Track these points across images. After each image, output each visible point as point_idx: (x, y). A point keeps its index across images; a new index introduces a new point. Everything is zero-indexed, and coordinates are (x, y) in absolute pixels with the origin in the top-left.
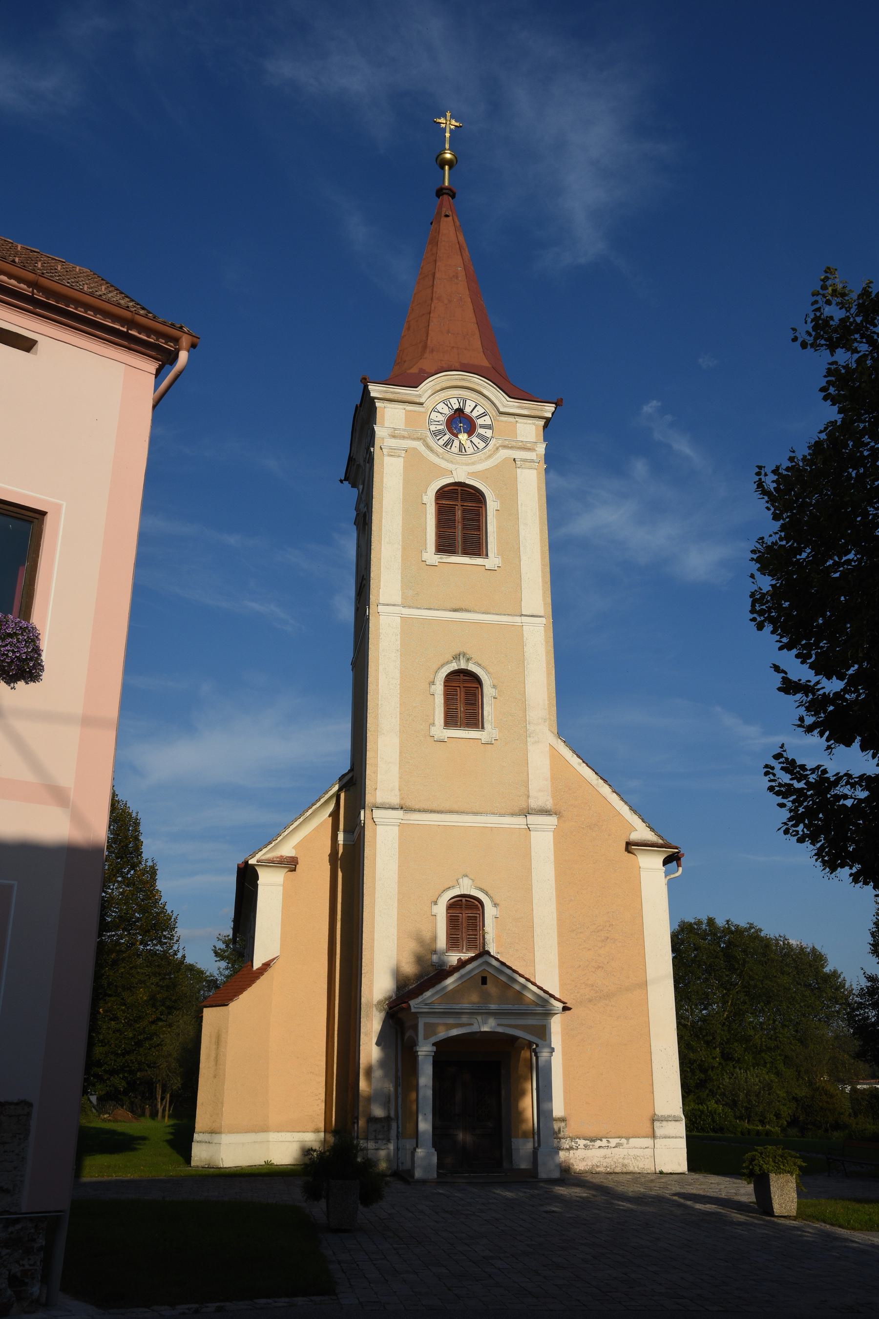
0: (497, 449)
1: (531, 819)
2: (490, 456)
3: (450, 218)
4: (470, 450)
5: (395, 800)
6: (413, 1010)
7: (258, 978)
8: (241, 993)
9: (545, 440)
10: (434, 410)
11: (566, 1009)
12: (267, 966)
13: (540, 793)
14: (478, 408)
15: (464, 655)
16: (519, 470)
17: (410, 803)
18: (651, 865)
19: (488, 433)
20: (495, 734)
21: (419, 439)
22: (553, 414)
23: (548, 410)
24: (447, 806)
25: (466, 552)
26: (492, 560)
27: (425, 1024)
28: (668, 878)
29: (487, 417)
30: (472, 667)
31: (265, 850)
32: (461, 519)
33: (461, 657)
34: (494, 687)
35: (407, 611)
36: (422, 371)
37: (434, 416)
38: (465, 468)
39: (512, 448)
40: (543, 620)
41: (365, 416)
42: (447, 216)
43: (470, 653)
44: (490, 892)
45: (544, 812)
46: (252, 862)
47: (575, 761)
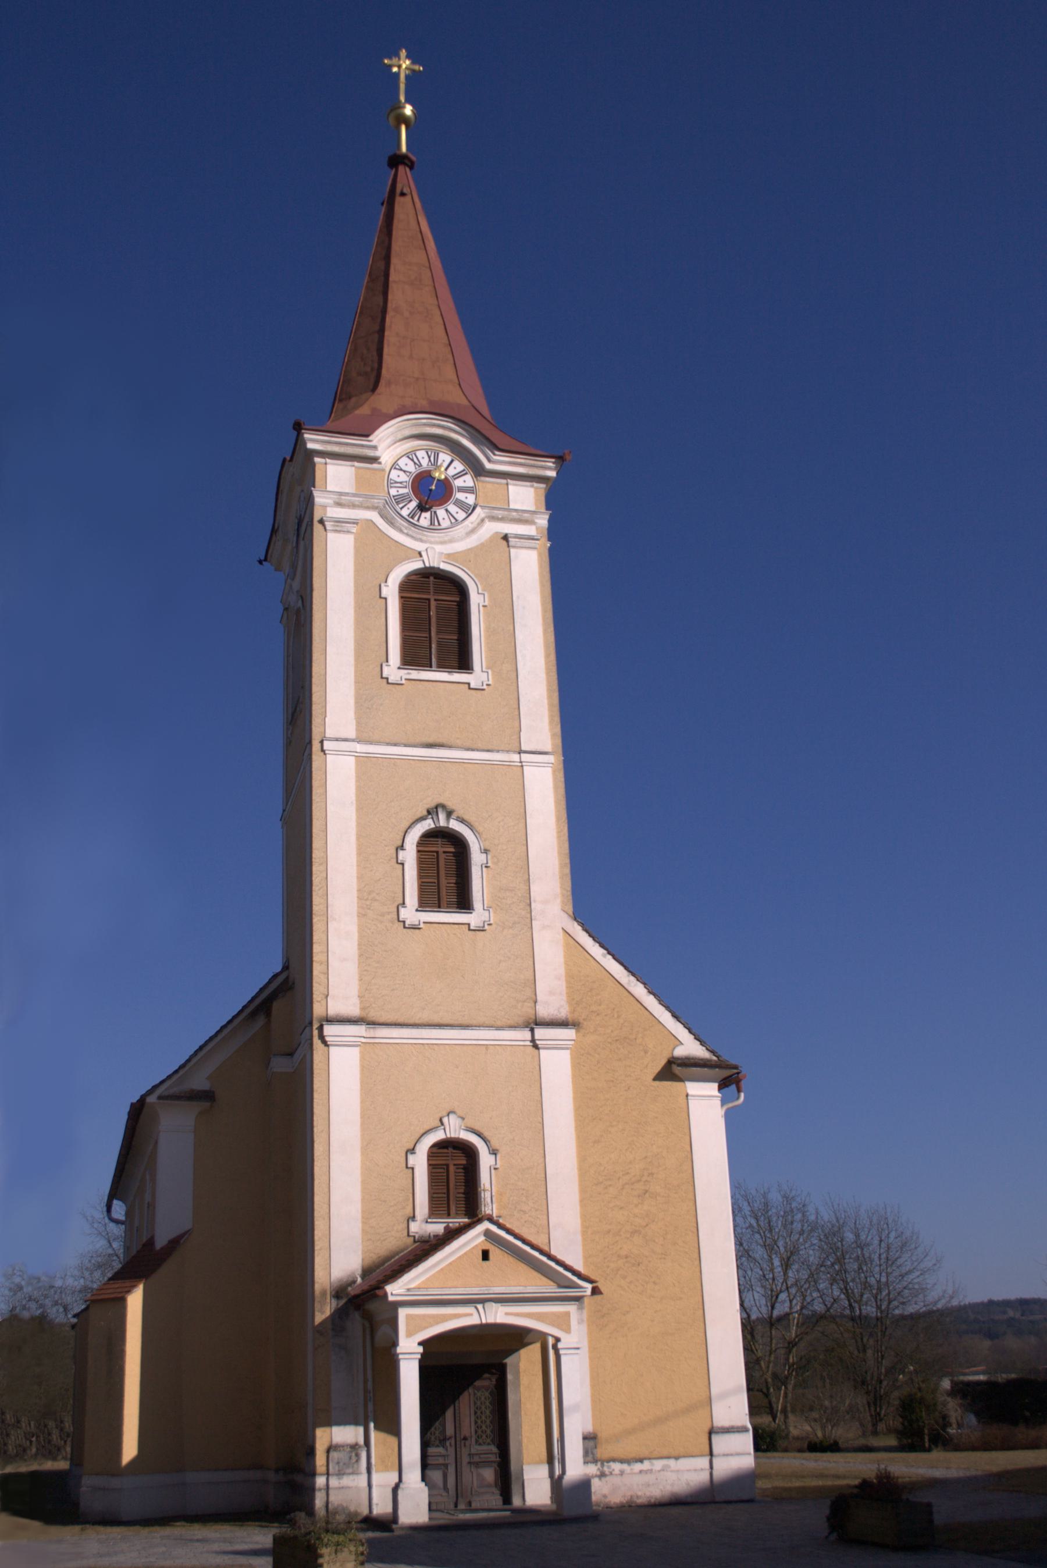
0: (483, 520)
1: (540, 1033)
2: (473, 531)
3: (408, 198)
4: (445, 523)
5: (353, 1009)
9: (548, 507)
10: (395, 466)
11: (595, 1291)
12: (175, 1244)
15: (443, 806)
17: (373, 1015)
18: (705, 1103)
19: (470, 499)
21: (374, 508)
24: (425, 1017)
25: (443, 666)
26: (476, 677)
27: (568, 1314)
28: (725, 1107)
30: (454, 825)
32: (437, 620)
33: (440, 810)
34: (486, 851)
35: (360, 748)
36: (375, 411)
37: (394, 475)
38: (439, 548)
39: (502, 520)
40: (551, 758)
41: (296, 478)
42: (403, 194)
43: (450, 805)
44: (486, 1134)
45: (563, 1024)
47: (596, 951)
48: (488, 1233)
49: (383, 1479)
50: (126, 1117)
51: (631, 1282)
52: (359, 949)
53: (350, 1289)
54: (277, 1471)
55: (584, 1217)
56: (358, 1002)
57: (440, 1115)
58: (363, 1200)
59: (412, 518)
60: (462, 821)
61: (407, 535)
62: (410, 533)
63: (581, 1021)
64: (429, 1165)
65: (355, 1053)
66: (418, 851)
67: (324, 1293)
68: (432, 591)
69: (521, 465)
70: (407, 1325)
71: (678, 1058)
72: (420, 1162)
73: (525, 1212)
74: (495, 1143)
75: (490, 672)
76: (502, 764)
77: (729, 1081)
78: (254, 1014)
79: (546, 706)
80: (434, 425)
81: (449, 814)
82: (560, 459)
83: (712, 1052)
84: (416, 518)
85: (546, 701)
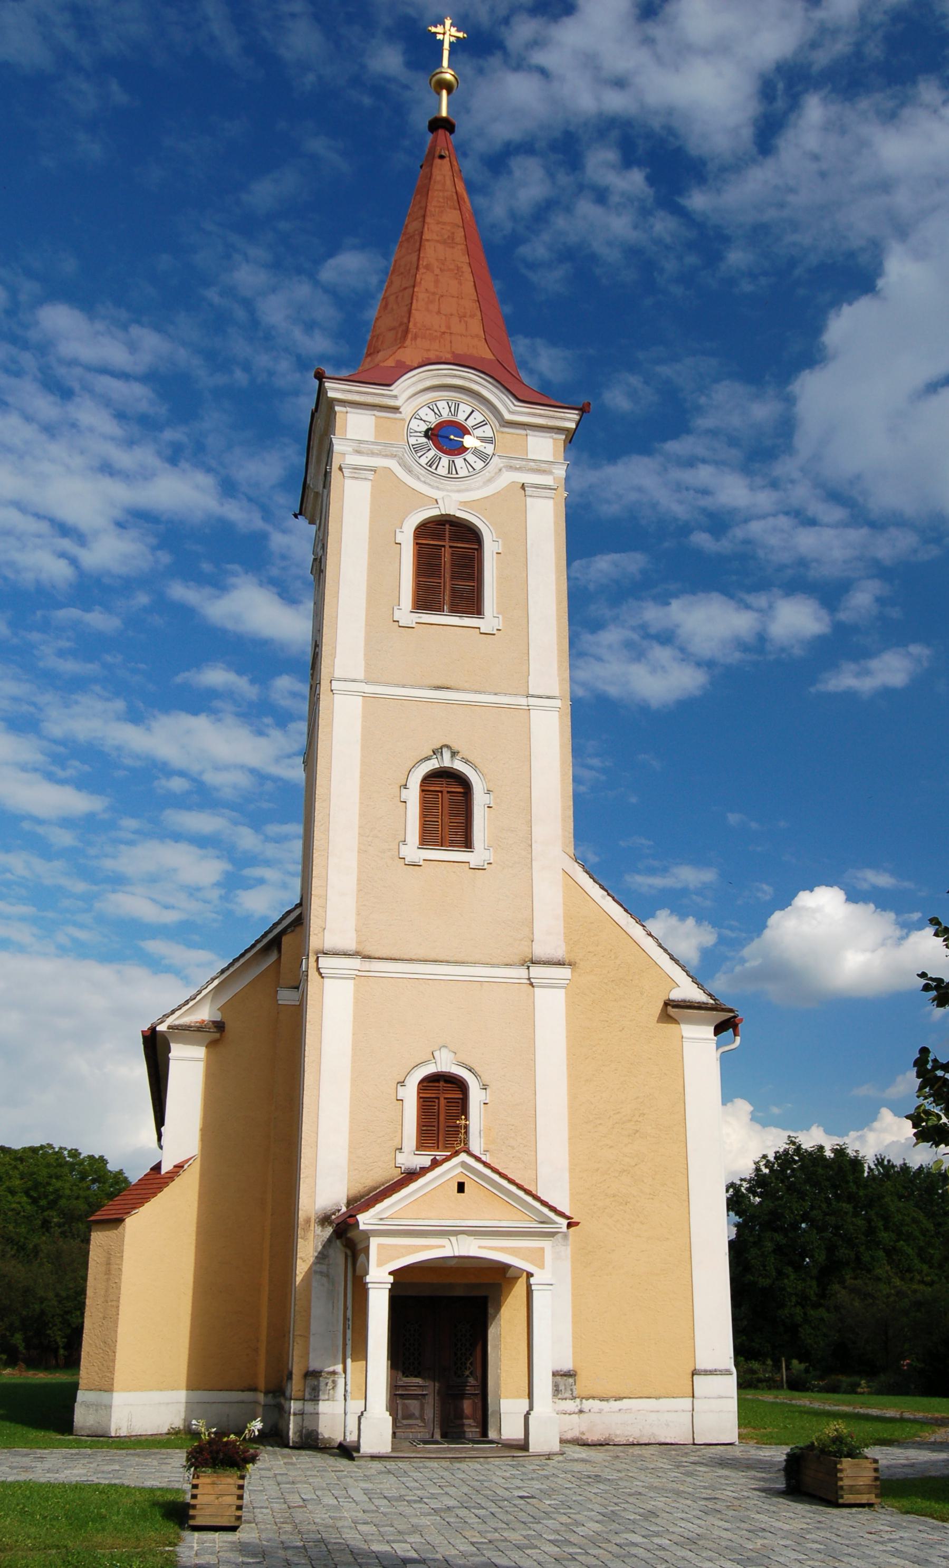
1: (536, 971)
2: (490, 480)
4: (463, 472)
5: (351, 946)
6: (362, 1227)
7: (167, 1184)
8: (142, 1204)
10: (415, 416)
13: (549, 939)
14: (476, 414)
15: (448, 747)
16: (528, 499)
17: (369, 950)
18: (699, 1043)
20: (488, 856)
21: (393, 456)
22: (577, 426)
23: (569, 419)
24: (421, 954)
25: (456, 610)
26: (490, 619)
27: (542, 1249)
28: (721, 1050)
29: (488, 427)
30: (459, 766)
31: (178, 1013)
32: (449, 564)
33: (445, 750)
37: (415, 424)
40: (558, 703)
42: (442, 157)
43: (456, 747)
44: (477, 1069)
45: (560, 964)
46: (162, 1028)
48: (464, 1164)
49: (355, 1406)
50: (142, 1046)
51: (618, 1221)
52: (358, 884)
53: (333, 1217)
54: (266, 1393)
55: (572, 1154)
56: (355, 936)
57: (432, 1049)
58: (352, 1131)
59: (430, 466)
60: (466, 761)
61: (425, 482)
62: (428, 481)
63: (578, 961)
64: (419, 1098)
65: (348, 986)
66: (423, 791)
67: (308, 1221)
68: (447, 538)
69: (541, 416)
70: (379, 1254)
71: (673, 1001)
72: (410, 1095)
73: (513, 1148)
74: (486, 1079)
75: (500, 616)
76: (510, 707)
77: (726, 1026)
78: (267, 949)
79: (556, 652)
80: (455, 376)
81: (454, 754)
82: (583, 410)
83: (710, 995)
84: (434, 467)
85: (556, 647)
